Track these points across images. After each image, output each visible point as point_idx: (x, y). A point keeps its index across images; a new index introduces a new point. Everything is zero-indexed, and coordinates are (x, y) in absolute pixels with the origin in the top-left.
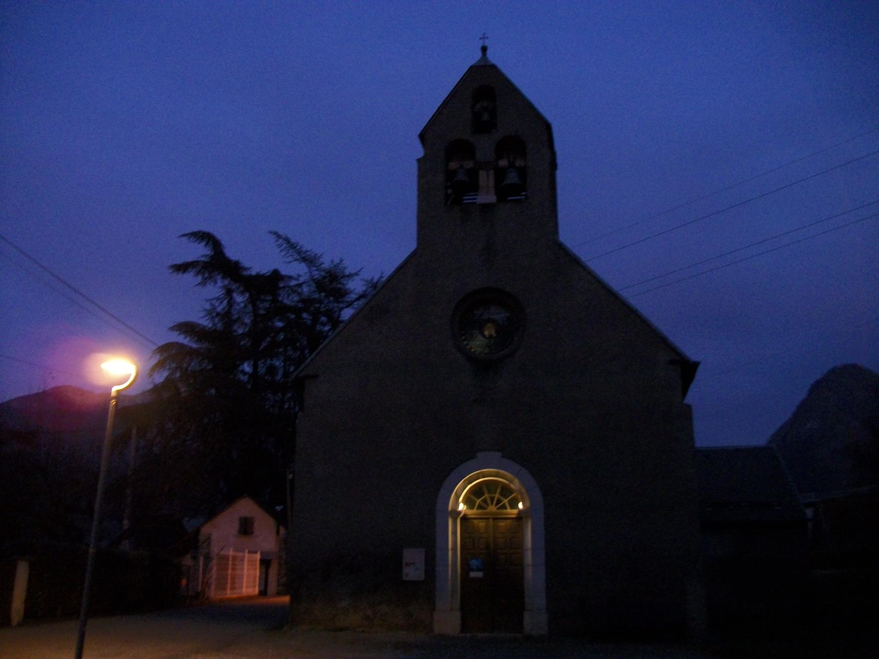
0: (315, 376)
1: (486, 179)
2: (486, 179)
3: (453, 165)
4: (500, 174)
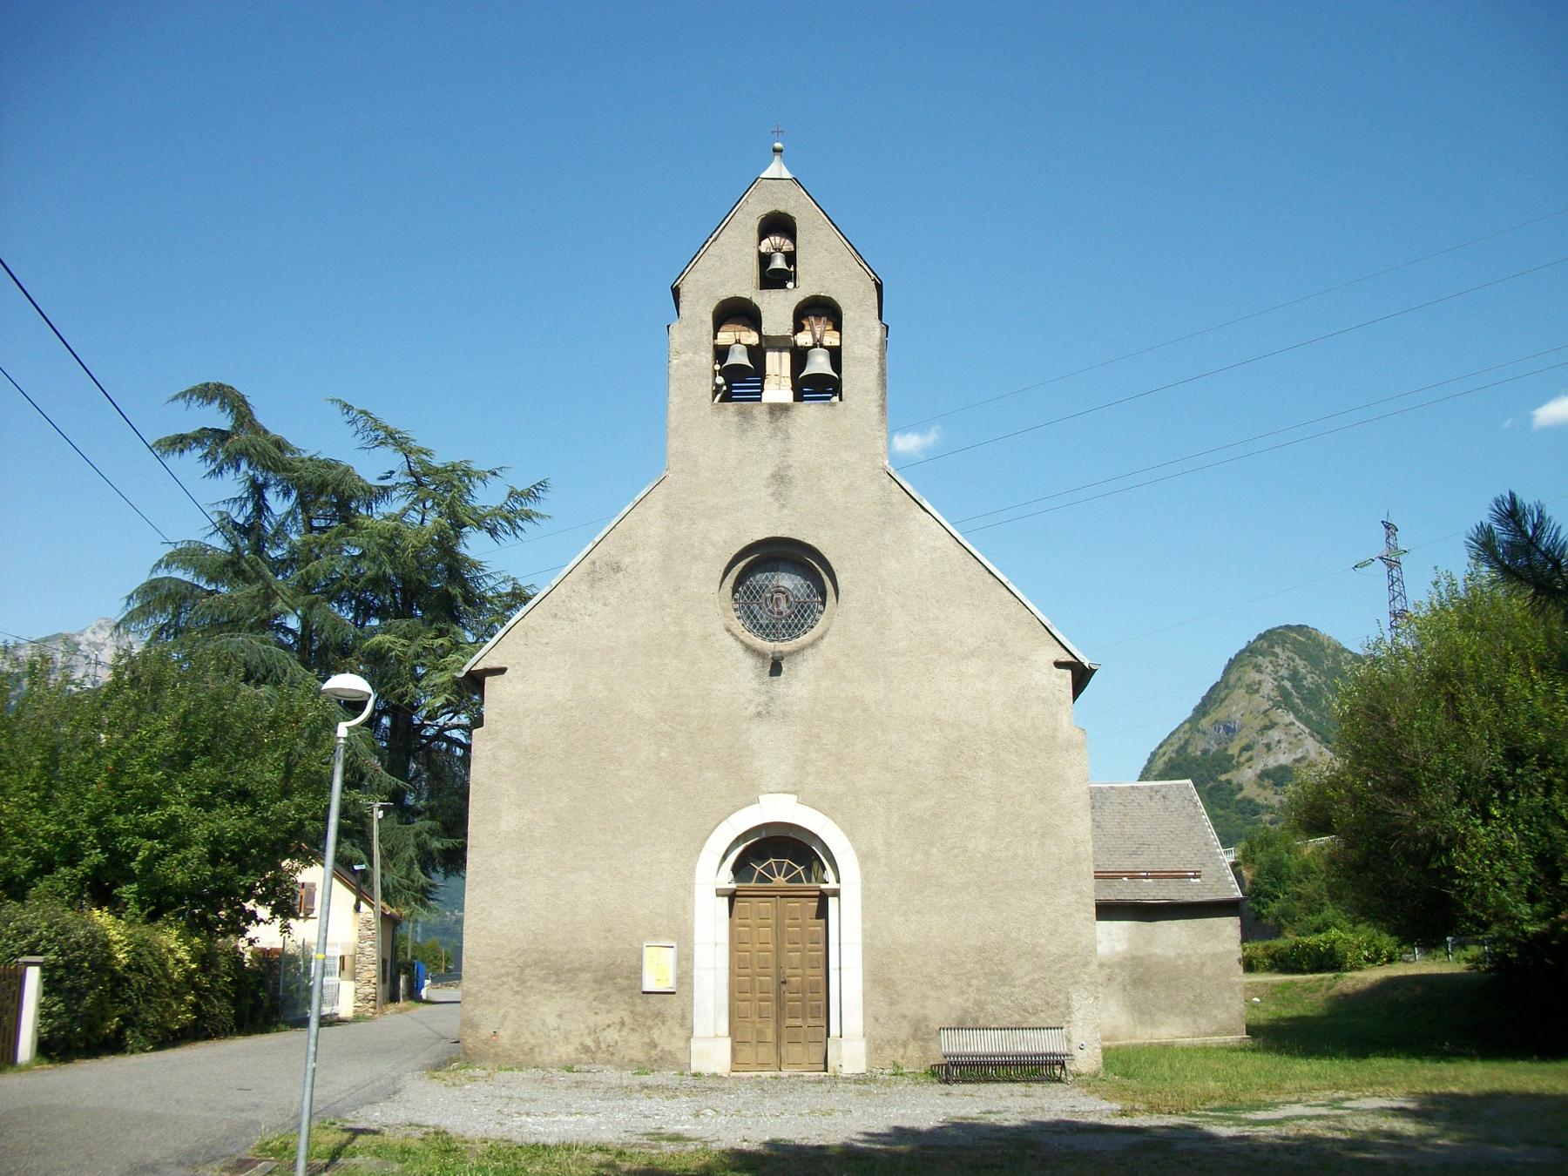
0: (502, 671)
1: (778, 364)
2: (778, 364)
3: (725, 337)
4: (800, 357)
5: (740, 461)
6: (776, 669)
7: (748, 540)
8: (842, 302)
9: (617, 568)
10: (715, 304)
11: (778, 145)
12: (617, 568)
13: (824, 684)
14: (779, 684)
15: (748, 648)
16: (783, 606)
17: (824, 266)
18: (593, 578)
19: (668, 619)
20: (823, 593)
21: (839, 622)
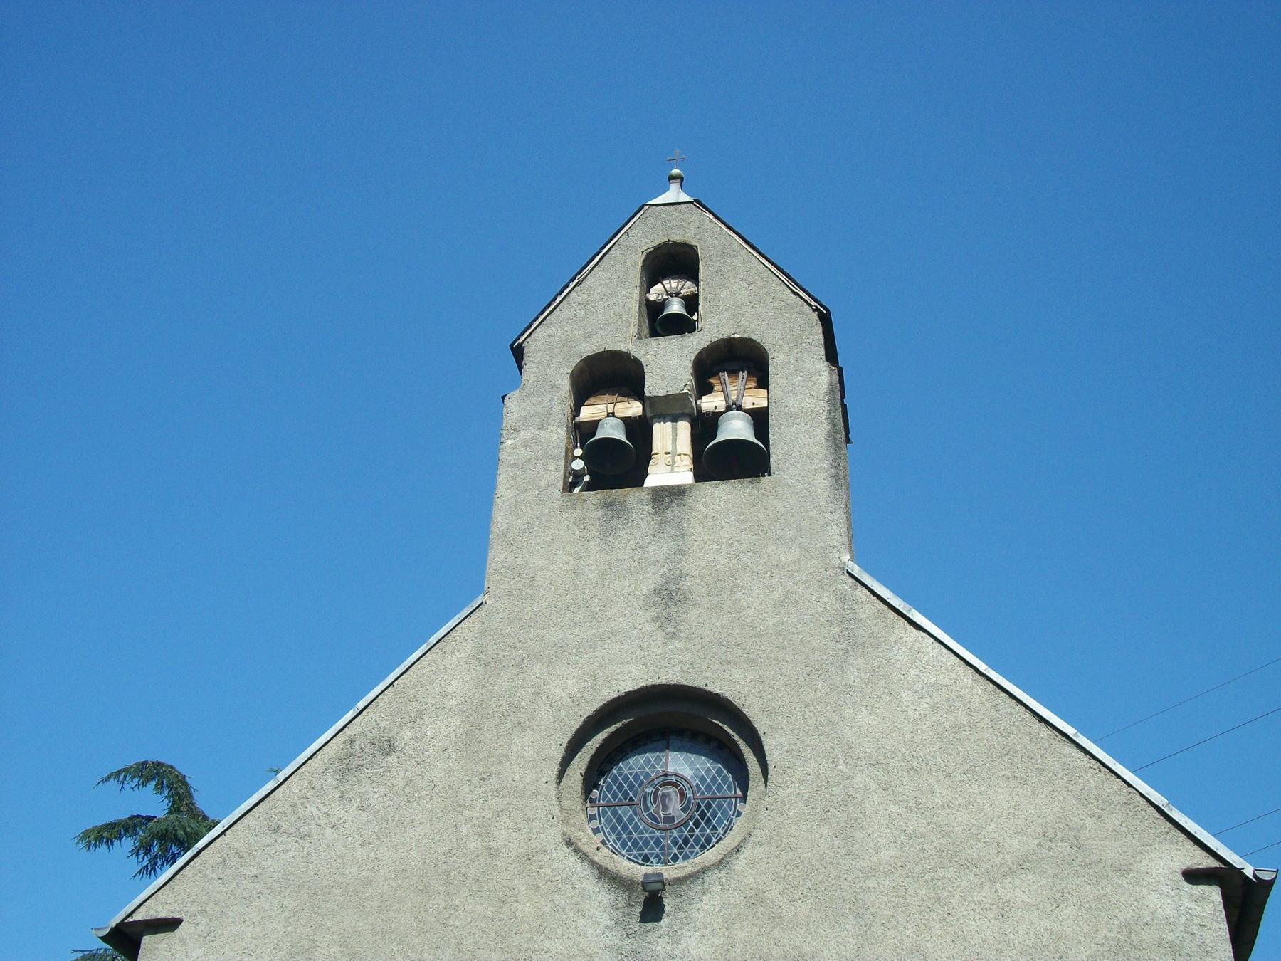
4: (705, 426)
5: (603, 574)
6: (652, 909)
7: (610, 693)
8: (768, 341)
9: (388, 748)
10: (575, 362)
11: (675, 172)
12: (388, 748)
13: (742, 934)
14: (658, 938)
15: (604, 874)
16: (675, 808)
17: (737, 296)
18: (347, 767)
19: (465, 829)
20: (743, 780)
21: (775, 824)
